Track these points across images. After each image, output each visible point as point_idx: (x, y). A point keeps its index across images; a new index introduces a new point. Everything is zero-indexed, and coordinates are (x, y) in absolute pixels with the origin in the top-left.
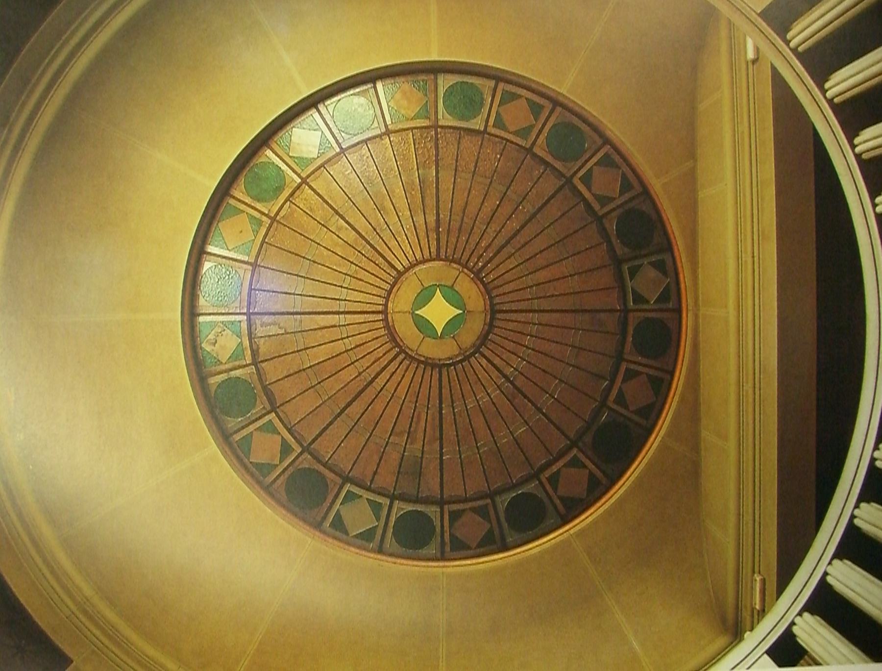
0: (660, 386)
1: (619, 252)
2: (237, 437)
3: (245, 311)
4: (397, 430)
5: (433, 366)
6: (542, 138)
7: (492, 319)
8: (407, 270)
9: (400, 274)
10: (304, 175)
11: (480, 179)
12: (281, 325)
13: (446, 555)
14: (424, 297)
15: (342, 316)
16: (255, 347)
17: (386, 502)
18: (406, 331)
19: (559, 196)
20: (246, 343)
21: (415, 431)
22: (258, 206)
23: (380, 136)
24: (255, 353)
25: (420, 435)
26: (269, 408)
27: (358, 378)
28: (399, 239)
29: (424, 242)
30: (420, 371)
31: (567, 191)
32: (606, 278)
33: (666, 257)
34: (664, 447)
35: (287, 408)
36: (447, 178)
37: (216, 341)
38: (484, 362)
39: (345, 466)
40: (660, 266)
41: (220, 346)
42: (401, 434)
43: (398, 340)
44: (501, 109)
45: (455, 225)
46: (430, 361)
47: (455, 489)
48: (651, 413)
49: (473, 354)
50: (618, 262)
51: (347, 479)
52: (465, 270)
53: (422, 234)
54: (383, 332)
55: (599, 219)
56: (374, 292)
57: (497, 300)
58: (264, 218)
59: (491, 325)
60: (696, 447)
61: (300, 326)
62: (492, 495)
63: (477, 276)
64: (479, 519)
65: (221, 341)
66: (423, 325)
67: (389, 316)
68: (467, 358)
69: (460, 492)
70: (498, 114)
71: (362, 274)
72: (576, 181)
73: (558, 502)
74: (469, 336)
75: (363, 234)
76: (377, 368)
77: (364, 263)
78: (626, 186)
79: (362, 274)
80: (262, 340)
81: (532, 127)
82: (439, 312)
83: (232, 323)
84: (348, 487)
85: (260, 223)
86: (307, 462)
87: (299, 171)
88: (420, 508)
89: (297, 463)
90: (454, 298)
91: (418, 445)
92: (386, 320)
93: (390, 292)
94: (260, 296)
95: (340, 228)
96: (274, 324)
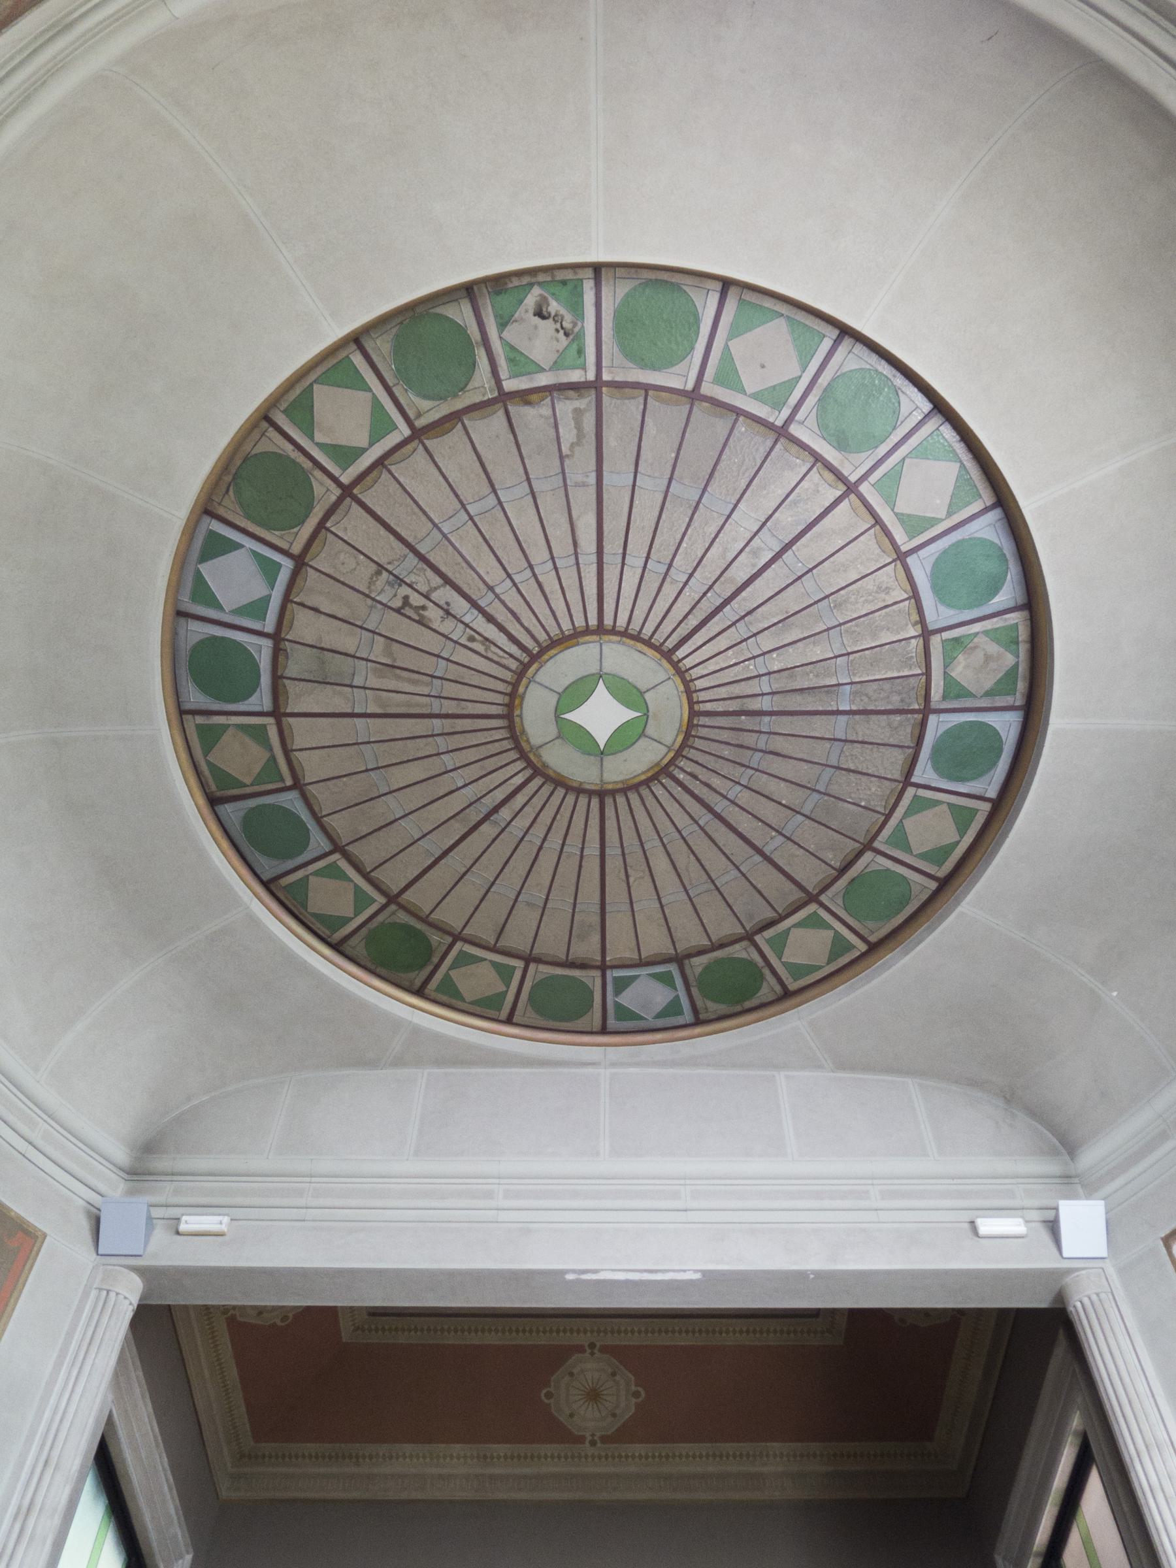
0: (488, 1009)
1: (696, 961)
2: (358, 359)
3: (606, 377)
4: (395, 646)
5: (510, 706)
6: (889, 864)
7: (590, 793)
8: (675, 665)
9: (668, 655)
10: (864, 488)
11: (826, 777)
12: (577, 449)
13: (190, 717)
14: (627, 693)
15: (594, 558)
16: (534, 397)
17: (269, 626)
18: (563, 668)
19: (789, 885)
20: (543, 380)
21: (399, 678)
22: (812, 400)
23: (922, 621)
24: (525, 397)
25: (392, 684)
26: (419, 423)
27: (482, 586)
28: (730, 652)
29: (723, 692)
30: (501, 687)
31: (798, 895)
32: (655, 942)
33: (688, 1017)
34: (397, 1024)
35: (420, 457)
36: (839, 727)
37: (543, 317)
38: (518, 780)
39: (321, 561)
40: (673, 1008)
41: (536, 327)
42: (388, 652)
43: (553, 652)
44: (945, 807)
45: (749, 739)
46: (517, 702)
47: (302, 732)
48: (449, 998)
49: (530, 764)
50: (680, 960)
51: (300, 562)
52: (672, 754)
53: (736, 690)
54: (566, 626)
55: (749, 937)
56: (636, 612)
57: (621, 800)
58: (786, 413)
59: (579, 791)
60: (398, 1062)
61: (577, 485)
62: (298, 785)
63: (662, 772)
64: (257, 768)
65: (547, 327)
66: (578, 692)
67: (595, 638)
68: (523, 756)
69: (298, 742)
70: (937, 803)
71: (669, 591)
72: (813, 907)
73: (300, 874)
74: (561, 759)
75: (744, 594)
76: (502, 616)
77: (690, 595)
78: (216, 547)
79: (669, 591)
80: (549, 412)
81: (908, 849)
82: (601, 716)
83: (581, 352)
84: (287, 565)
85: (778, 406)
86: (325, 492)
87: (873, 478)
88: (265, 680)
89: (318, 473)
90: (624, 738)
91: (373, 682)
92: (587, 631)
93: (637, 638)
94: (634, 407)
95: (756, 553)
96: (580, 435)
